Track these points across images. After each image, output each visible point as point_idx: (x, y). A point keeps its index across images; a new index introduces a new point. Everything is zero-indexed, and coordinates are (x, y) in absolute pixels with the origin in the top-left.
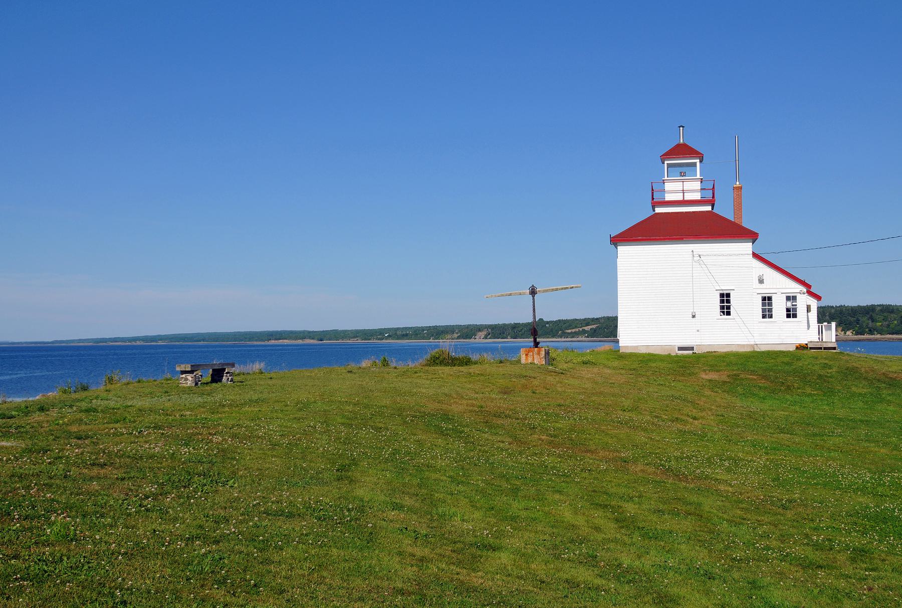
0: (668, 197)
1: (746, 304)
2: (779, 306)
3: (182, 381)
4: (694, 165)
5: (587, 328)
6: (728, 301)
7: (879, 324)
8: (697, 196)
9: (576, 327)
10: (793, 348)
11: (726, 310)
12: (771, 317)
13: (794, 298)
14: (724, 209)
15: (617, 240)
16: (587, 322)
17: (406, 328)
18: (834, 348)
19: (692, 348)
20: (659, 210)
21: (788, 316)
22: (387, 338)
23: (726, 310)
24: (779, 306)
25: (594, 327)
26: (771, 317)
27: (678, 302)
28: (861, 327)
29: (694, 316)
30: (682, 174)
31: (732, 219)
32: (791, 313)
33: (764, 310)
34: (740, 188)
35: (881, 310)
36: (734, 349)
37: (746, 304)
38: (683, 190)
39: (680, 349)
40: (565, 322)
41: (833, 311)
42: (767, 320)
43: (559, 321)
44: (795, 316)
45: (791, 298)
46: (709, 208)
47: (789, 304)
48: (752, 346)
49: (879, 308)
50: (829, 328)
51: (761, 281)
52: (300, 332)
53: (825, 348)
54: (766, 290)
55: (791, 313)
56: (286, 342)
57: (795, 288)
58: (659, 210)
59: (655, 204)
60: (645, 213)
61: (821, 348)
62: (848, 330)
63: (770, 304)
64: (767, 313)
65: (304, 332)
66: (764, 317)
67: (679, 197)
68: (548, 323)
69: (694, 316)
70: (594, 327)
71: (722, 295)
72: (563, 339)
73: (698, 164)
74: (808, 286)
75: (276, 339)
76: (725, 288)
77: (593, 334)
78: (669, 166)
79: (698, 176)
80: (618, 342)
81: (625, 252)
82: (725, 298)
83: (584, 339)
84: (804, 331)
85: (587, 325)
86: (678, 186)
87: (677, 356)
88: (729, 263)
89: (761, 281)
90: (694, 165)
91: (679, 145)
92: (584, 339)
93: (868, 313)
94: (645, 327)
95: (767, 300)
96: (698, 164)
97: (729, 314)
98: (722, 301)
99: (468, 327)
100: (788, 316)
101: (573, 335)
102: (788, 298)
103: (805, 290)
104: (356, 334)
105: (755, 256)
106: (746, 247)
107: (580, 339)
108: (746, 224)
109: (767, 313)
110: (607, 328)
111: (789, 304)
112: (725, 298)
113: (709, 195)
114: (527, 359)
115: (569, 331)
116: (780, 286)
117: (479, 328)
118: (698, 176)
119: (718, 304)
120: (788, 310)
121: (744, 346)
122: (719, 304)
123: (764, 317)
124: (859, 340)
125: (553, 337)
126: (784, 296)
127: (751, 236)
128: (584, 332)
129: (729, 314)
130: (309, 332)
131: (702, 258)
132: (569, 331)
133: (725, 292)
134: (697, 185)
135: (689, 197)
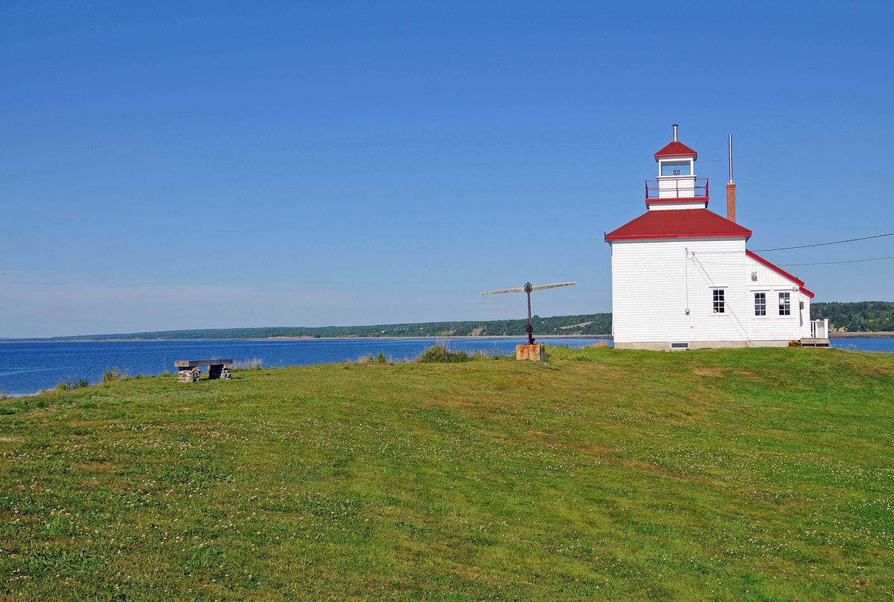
0: (662, 195)
1: (740, 301)
2: (772, 303)
3: (181, 377)
4: (688, 163)
5: (582, 325)
6: (722, 298)
7: (871, 321)
8: (691, 194)
9: (571, 324)
11: (719, 307)
12: (764, 313)
13: (787, 295)
14: (718, 207)
15: (611, 238)
16: (582, 319)
17: (402, 325)
18: (827, 345)
19: (686, 345)
20: (653, 208)
21: (781, 313)
22: (384, 335)
23: (719, 307)
24: (772, 303)
26: (764, 313)
27: (671, 298)
28: (853, 324)
29: (687, 313)
30: (676, 172)
32: (784, 310)
33: (757, 307)
35: (873, 307)
36: (728, 346)
37: (740, 301)
38: (677, 188)
39: (674, 345)
40: (560, 318)
41: (826, 308)
42: (760, 316)
43: (554, 317)
44: (788, 313)
45: (784, 295)
46: (702, 206)
47: (782, 301)
48: (746, 342)
49: (871, 305)
50: (822, 325)
51: (754, 278)
52: (297, 329)
53: (818, 345)
54: (759, 287)
55: (784, 310)
56: (283, 338)
57: (788, 285)
58: (653, 208)
59: (649, 202)
60: (641, 211)
61: (813, 345)
62: (841, 326)
63: (763, 301)
64: (760, 310)
65: (301, 328)
66: (757, 313)
67: (672, 195)
68: (543, 319)
69: (687, 313)
71: (715, 292)
72: (558, 336)
73: (692, 163)
74: (801, 283)
75: (273, 336)
76: (719, 285)
77: (588, 330)
78: (663, 164)
79: (692, 175)
80: (612, 338)
81: (620, 249)
82: (719, 295)
83: (578, 335)
84: (798, 328)
85: (582, 322)
86: (672, 184)
87: (671, 353)
88: (723, 261)
89: (754, 278)
90: (688, 163)
91: (673, 144)
92: (578, 335)
93: (860, 310)
95: (760, 297)
96: (692, 163)
97: (722, 310)
98: (715, 298)
99: (464, 323)
100: (781, 313)
101: (568, 332)
102: (781, 295)
103: (798, 287)
105: (749, 253)
106: (740, 245)
107: (575, 335)
108: (739, 222)
109: (760, 310)
110: (603, 324)
111: (782, 301)
112: (719, 295)
113: (702, 193)
114: (522, 355)
115: (564, 328)
116: (773, 283)
117: (475, 325)
118: (692, 175)
119: (711, 301)
120: (781, 307)
121: (737, 342)
122: (712, 301)
123: (757, 313)
124: (852, 337)
125: (548, 333)
126: (777, 294)
127: (745, 234)
128: (579, 328)
129: (722, 310)
130: (307, 329)
131: (696, 255)
132: (564, 328)
133: (719, 289)
134: (691, 183)
135: (683, 195)
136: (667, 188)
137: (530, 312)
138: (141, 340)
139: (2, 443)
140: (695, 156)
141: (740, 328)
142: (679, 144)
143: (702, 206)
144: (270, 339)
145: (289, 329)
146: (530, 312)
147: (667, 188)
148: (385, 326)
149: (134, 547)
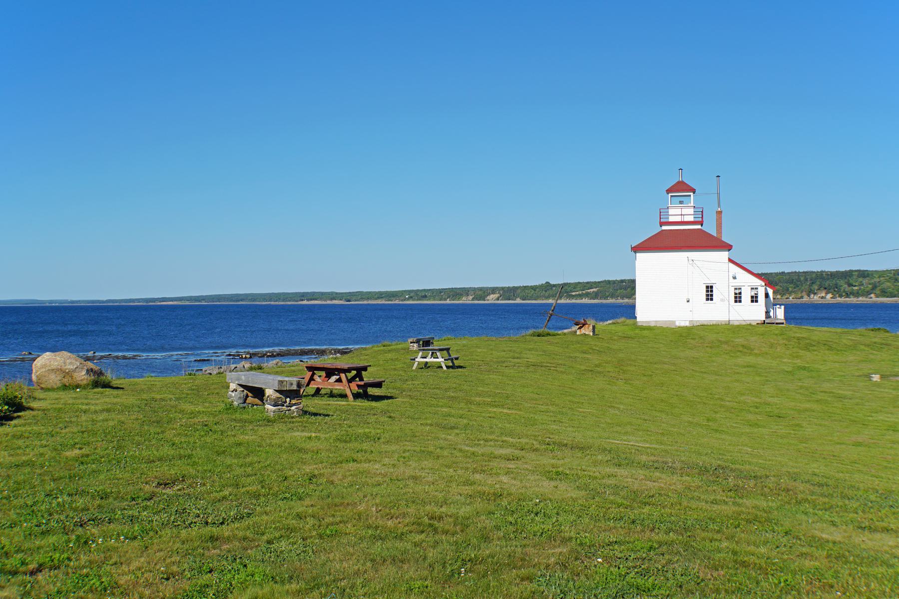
0: (671, 219)
2: (746, 296)
6: (712, 291)
8: (691, 219)
11: (710, 297)
14: (710, 228)
15: (637, 249)
16: (590, 285)
20: (664, 228)
21: (752, 301)
25: (595, 290)
27: (674, 292)
30: (681, 202)
31: (714, 234)
32: (754, 299)
34: (720, 212)
38: (681, 213)
41: (814, 276)
44: (757, 301)
46: (699, 227)
47: (737, 291)
51: (735, 278)
54: (737, 283)
55: (754, 299)
58: (664, 228)
59: (662, 224)
60: (657, 229)
64: (738, 299)
66: (707, 299)
67: (678, 219)
68: (554, 286)
70: (595, 290)
71: (707, 287)
75: (308, 300)
76: (709, 282)
80: (636, 318)
81: (640, 256)
82: (710, 289)
84: (755, 313)
86: (678, 211)
88: (712, 265)
91: (679, 182)
98: (707, 291)
99: (481, 289)
100: (752, 301)
105: (730, 260)
106: (724, 255)
108: (725, 239)
109: (738, 299)
110: (630, 311)
112: (710, 289)
116: (747, 282)
117: (494, 290)
119: (704, 293)
120: (752, 297)
127: (728, 247)
130: (337, 293)
134: (691, 211)
135: (687, 219)
138: (187, 303)
140: (694, 191)
141: (722, 311)
143: (699, 227)
144: (305, 302)
145: (322, 294)
148: (410, 292)
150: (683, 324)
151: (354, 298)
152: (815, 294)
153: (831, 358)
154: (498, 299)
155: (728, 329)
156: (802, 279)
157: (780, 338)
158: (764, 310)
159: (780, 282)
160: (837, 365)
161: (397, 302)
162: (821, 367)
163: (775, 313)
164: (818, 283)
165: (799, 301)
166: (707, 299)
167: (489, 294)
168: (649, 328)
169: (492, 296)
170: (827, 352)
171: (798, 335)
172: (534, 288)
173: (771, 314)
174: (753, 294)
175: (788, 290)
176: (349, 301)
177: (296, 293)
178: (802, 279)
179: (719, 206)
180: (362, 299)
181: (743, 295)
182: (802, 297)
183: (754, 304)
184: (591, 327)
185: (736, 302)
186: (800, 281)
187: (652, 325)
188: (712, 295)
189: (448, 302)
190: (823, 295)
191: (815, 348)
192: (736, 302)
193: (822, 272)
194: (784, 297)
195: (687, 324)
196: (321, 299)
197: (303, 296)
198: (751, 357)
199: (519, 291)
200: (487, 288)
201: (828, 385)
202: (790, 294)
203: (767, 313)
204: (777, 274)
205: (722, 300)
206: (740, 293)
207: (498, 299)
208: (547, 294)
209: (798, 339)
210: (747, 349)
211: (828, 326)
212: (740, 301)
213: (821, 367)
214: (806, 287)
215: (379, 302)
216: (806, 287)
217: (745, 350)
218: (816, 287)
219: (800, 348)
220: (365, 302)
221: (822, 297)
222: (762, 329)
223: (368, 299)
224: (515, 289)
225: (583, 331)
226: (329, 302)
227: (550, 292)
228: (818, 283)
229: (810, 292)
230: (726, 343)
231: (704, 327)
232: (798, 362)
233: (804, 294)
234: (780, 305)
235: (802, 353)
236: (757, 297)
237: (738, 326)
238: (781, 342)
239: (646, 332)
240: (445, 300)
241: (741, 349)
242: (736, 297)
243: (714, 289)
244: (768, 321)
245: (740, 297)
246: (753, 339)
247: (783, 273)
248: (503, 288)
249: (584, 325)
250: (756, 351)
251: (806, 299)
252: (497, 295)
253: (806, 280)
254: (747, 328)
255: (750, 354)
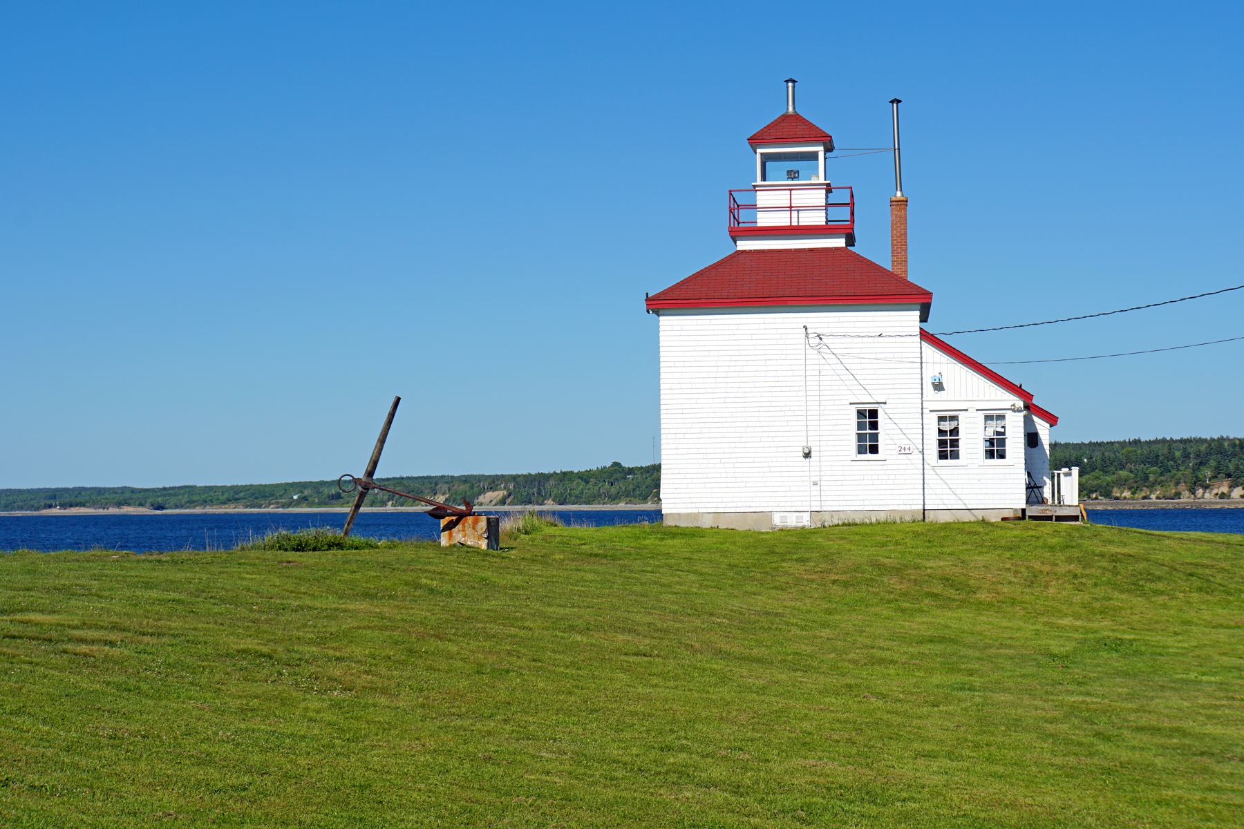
0: (764, 220)
2: (972, 439)
4: (813, 156)
6: (874, 426)
8: (818, 219)
10: (908, 518)
14: (874, 247)
15: (662, 304)
17: (210, 488)
18: (1075, 518)
20: (743, 245)
21: (990, 454)
22: (298, 503)
26: (1002, 456)
27: (766, 426)
29: (807, 455)
30: (792, 175)
31: (886, 263)
38: (790, 205)
41: (1203, 448)
46: (840, 242)
47: (947, 426)
50: (1069, 474)
51: (938, 387)
52: (114, 491)
53: (1059, 518)
55: (995, 449)
58: (743, 245)
60: (721, 248)
64: (948, 447)
65: (123, 490)
66: (861, 450)
67: (782, 220)
75: (63, 506)
76: (867, 399)
78: (766, 158)
81: (680, 333)
82: (869, 418)
84: (998, 488)
86: (781, 198)
88: (875, 348)
90: (813, 156)
91: (785, 117)
94: (698, 487)
97: (874, 449)
99: (465, 479)
100: (990, 454)
103: (1020, 404)
104: (234, 494)
105: (925, 336)
108: (916, 276)
109: (948, 447)
110: (648, 480)
112: (869, 418)
113: (843, 214)
116: (972, 395)
117: (494, 482)
118: (822, 180)
119: (853, 430)
126: (981, 415)
127: (924, 305)
129: (874, 449)
130: (133, 491)
131: (825, 340)
134: (819, 197)
136: (775, 205)
137: (374, 463)
139: (1236, 479)
141: (899, 485)
142: (796, 117)
143: (840, 242)
145: (100, 491)
146: (374, 463)
147: (775, 205)
149: (656, 686)
150: (792, 521)
151: (173, 500)
152: (1206, 487)
153: (1207, 615)
154: (503, 502)
155: (916, 535)
156: (1178, 454)
157: (1061, 556)
158: (1022, 478)
159: (1129, 460)
160: (1222, 635)
161: (271, 509)
162: (1170, 641)
163: (1057, 490)
164: (1213, 463)
165: (1171, 504)
166: (861, 450)
167: (483, 491)
168: (693, 534)
169: (490, 495)
170: (1195, 596)
171: (1114, 549)
172: (585, 477)
173: (1047, 492)
174: (990, 434)
175: (1146, 478)
176: (161, 507)
177: (39, 490)
178: (1178, 454)
179: (899, 184)
180: (192, 503)
181: (962, 436)
182: (1178, 495)
183: (996, 461)
184: (483, 524)
185: (943, 456)
186: (1173, 459)
187: (707, 523)
188: (875, 437)
189: (389, 508)
190: (1225, 489)
191: (1160, 586)
192: (943, 456)
193: (1221, 439)
194: (1140, 495)
195: (805, 521)
196: (94, 504)
197: (53, 496)
198: (961, 613)
199: (552, 482)
200: (480, 478)
201: (1175, 701)
202: (1152, 487)
203: (1033, 489)
204: (1123, 444)
205: (904, 451)
206: (955, 431)
207: (503, 502)
208: (613, 490)
209: (1114, 558)
210: (957, 590)
211: (1208, 528)
212: (955, 456)
213: (1170, 641)
214: (1185, 472)
215: (230, 509)
216: (1185, 472)
217: (951, 592)
218: (1209, 473)
219: (1116, 587)
220: (198, 510)
221: (1223, 496)
222: (1017, 531)
223: (204, 503)
224: (542, 478)
225: (458, 535)
226: (113, 511)
227: (621, 485)
228: (1213, 463)
229: (1196, 484)
230: (898, 571)
231: (853, 531)
232: (1104, 627)
233: (1182, 487)
234: (1068, 465)
235: (1119, 599)
236: (1002, 442)
237: (946, 526)
238: (1063, 568)
239: (676, 542)
240: (384, 504)
241: (937, 589)
242: (942, 443)
243: (881, 419)
244: (1034, 510)
245: (955, 443)
246: (982, 559)
247: (1137, 442)
248: (514, 478)
249: (461, 516)
250: (983, 596)
251: (1186, 499)
252: (500, 494)
253: (1186, 456)
254: (974, 532)
255: (964, 603)
